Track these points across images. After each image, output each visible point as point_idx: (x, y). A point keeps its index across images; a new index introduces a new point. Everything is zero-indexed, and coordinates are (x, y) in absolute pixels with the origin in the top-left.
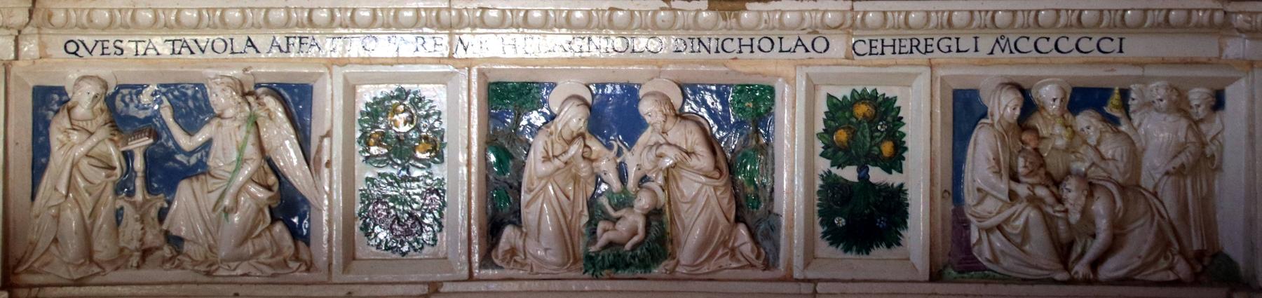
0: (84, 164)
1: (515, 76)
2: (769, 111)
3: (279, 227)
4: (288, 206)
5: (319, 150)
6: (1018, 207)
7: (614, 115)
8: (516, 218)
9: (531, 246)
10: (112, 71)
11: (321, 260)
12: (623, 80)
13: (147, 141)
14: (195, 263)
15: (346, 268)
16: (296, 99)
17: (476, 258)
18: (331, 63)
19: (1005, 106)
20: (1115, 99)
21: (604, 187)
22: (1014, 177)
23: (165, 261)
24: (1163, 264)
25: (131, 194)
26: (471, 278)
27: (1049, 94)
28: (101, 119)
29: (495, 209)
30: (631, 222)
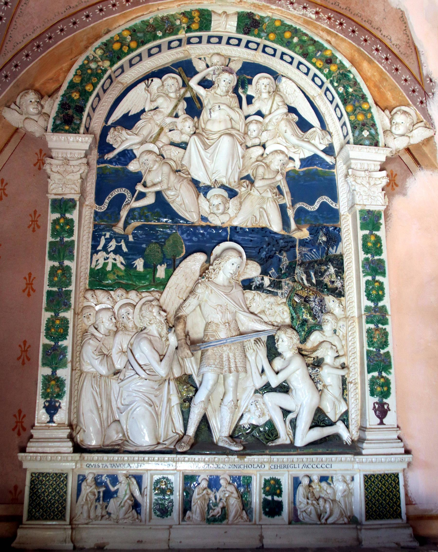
0: (89, 494)
1: (190, 474)
2: (250, 482)
3: (134, 511)
4: (136, 506)
5: (144, 492)
6: (309, 506)
7: (214, 483)
8: (190, 509)
9: (194, 516)
10: (96, 471)
11: (143, 519)
12: (216, 474)
13: (104, 489)
14: (114, 519)
15: (149, 521)
16: (139, 479)
17: (181, 519)
18: (147, 470)
19: (306, 481)
20: (330, 479)
21: (211, 502)
22: (308, 498)
23: (106, 519)
24: (342, 519)
25: (99, 501)
26: (179, 524)
27: (315, 478)
28: (94, 483)
29: (185, 507)
30: (218, 509)
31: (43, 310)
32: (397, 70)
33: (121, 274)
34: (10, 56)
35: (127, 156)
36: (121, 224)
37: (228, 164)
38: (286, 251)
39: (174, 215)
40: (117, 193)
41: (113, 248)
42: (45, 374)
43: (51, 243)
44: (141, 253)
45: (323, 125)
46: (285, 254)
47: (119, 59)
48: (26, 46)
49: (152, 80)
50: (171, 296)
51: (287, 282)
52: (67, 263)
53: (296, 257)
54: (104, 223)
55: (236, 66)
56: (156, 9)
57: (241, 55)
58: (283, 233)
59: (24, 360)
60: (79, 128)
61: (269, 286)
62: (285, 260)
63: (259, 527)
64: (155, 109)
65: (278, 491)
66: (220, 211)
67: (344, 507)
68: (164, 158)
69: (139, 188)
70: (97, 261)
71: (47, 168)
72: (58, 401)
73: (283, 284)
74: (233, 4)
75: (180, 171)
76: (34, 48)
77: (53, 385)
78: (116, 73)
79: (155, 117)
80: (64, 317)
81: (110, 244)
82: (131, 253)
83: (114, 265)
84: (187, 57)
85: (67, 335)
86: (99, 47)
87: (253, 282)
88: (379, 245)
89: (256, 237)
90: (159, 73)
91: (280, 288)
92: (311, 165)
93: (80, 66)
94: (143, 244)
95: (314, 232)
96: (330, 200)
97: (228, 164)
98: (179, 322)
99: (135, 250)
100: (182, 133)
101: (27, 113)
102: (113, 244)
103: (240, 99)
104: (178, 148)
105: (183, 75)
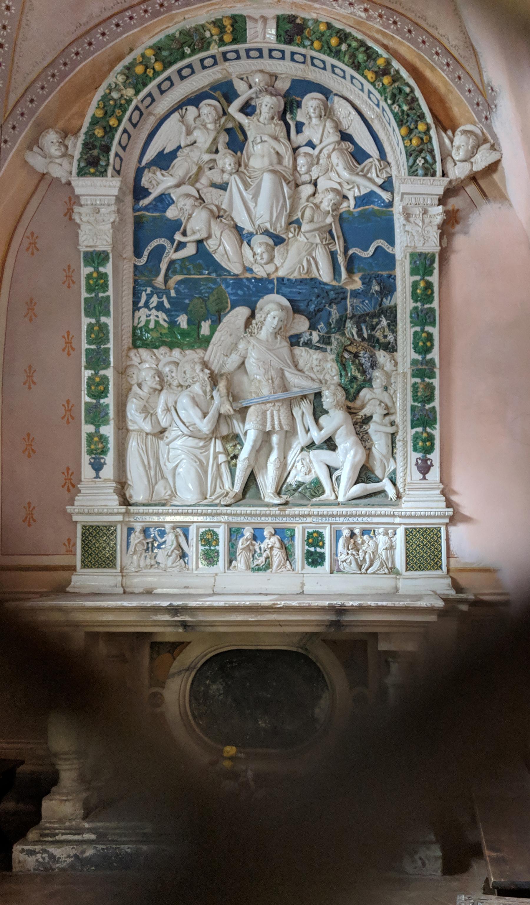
19: (346, 533)
31: (83, 368)
32: (459, 78)
33: (164, 331)
34: (22, 90)
35: (164, 200)
36: (161, 278)
37: (272, 207)
38: (336, 304)
39: (217, 268)
40: (156, 244)
41: (154, 304)
42: (89, 432)
43: (86, 299)
44: (184, 309)
45: (383, 155)
46: (334, 307)
47: (145, 85)
48: (39, 75)
49: (186, 109)
50: (214, 353)
51: (337, 337)
52: (103, 319)
53: (346, 310)
54: (143, 277)
55: (283, 85)
56: (182, 18)
57: (288, 70)
58: (334, 283)
59: (68, 419)
60: (106, 171)
61: (319, 342)
62: (335, 312)
63: (302, 575)
64: (192, 144)
65: (321, 544)
66: (264, 261)
67: (384, 558)
68: (204, 202)
69: (178, 237)
70: (139, 318)
71: (76, 217)
72: (103, 458)
73: (333, 340)
74: (270, 5)
75: (222, 216)
76: (49, 78)
77: (96, 442)
78: (144, 102)
79: (191, 154)
80: (104, 375)
81: (152, 300)
82: (173, 309)
83: (157, 322)
84: (226, 77)
85: (108, 392)
86: (122, 73)
87: (300, 338)
88: (429, 292)
89: (304, 289)
90: (195, 100)
91: (329, 343)
92: (367, 204)
93: (102, 97)
94: (185, 299)
95: (367, 281)
96: (386, 244)
97: (272, 207)
98: (222, 379)
99: (177, 306)
100: (223, 171)
101: (51, 157)
102: (154, 300)
103: (288, 127)
104: (219, 190)
105: (222, 100)
